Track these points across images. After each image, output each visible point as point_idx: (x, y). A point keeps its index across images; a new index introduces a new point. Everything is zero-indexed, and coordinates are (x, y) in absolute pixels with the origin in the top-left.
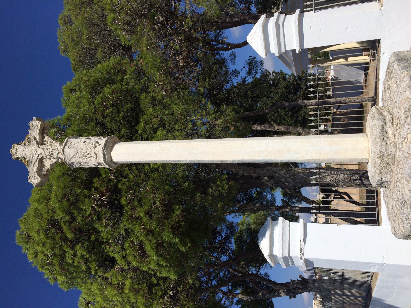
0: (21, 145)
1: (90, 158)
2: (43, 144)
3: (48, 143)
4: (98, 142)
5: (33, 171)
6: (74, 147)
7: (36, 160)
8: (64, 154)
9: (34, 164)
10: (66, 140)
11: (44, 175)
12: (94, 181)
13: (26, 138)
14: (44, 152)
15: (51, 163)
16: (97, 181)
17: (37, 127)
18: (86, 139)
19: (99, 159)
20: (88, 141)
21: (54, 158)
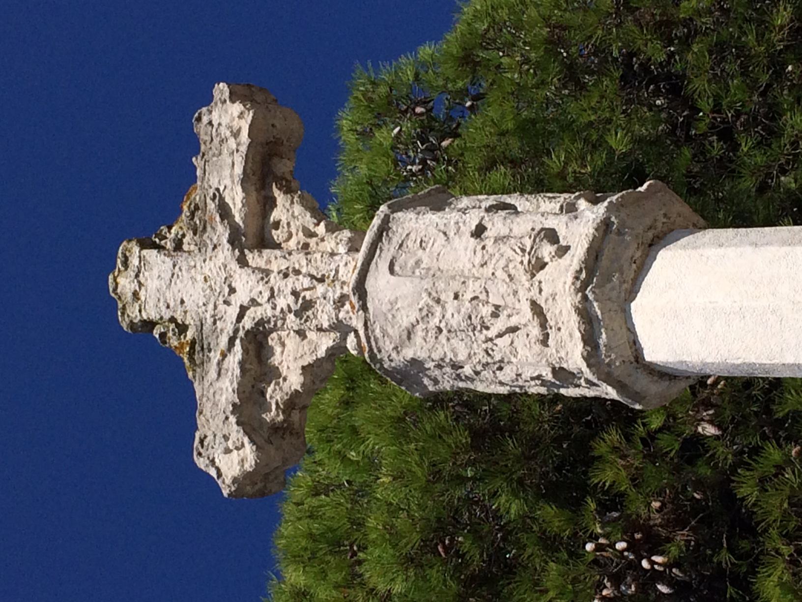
0: (159, 248)
1: (507, 339)
2: (264, 242)
3: (290, 236)
4: (551, 236)
5: (215, 404)
6: (418, 263)
7: (231, 342)
8: (364, 308)
9: (220, 364)
10: (376, 222)
11: (276, 429)
12: (601, 448)
13: (185, 208)
14: (266, 295)
15: (308, 360)
16: (615, 449)
17: (232, 143)
18: (488, 210)
19: (560, 345)
20: (497, 225)
21: (320, 329)
